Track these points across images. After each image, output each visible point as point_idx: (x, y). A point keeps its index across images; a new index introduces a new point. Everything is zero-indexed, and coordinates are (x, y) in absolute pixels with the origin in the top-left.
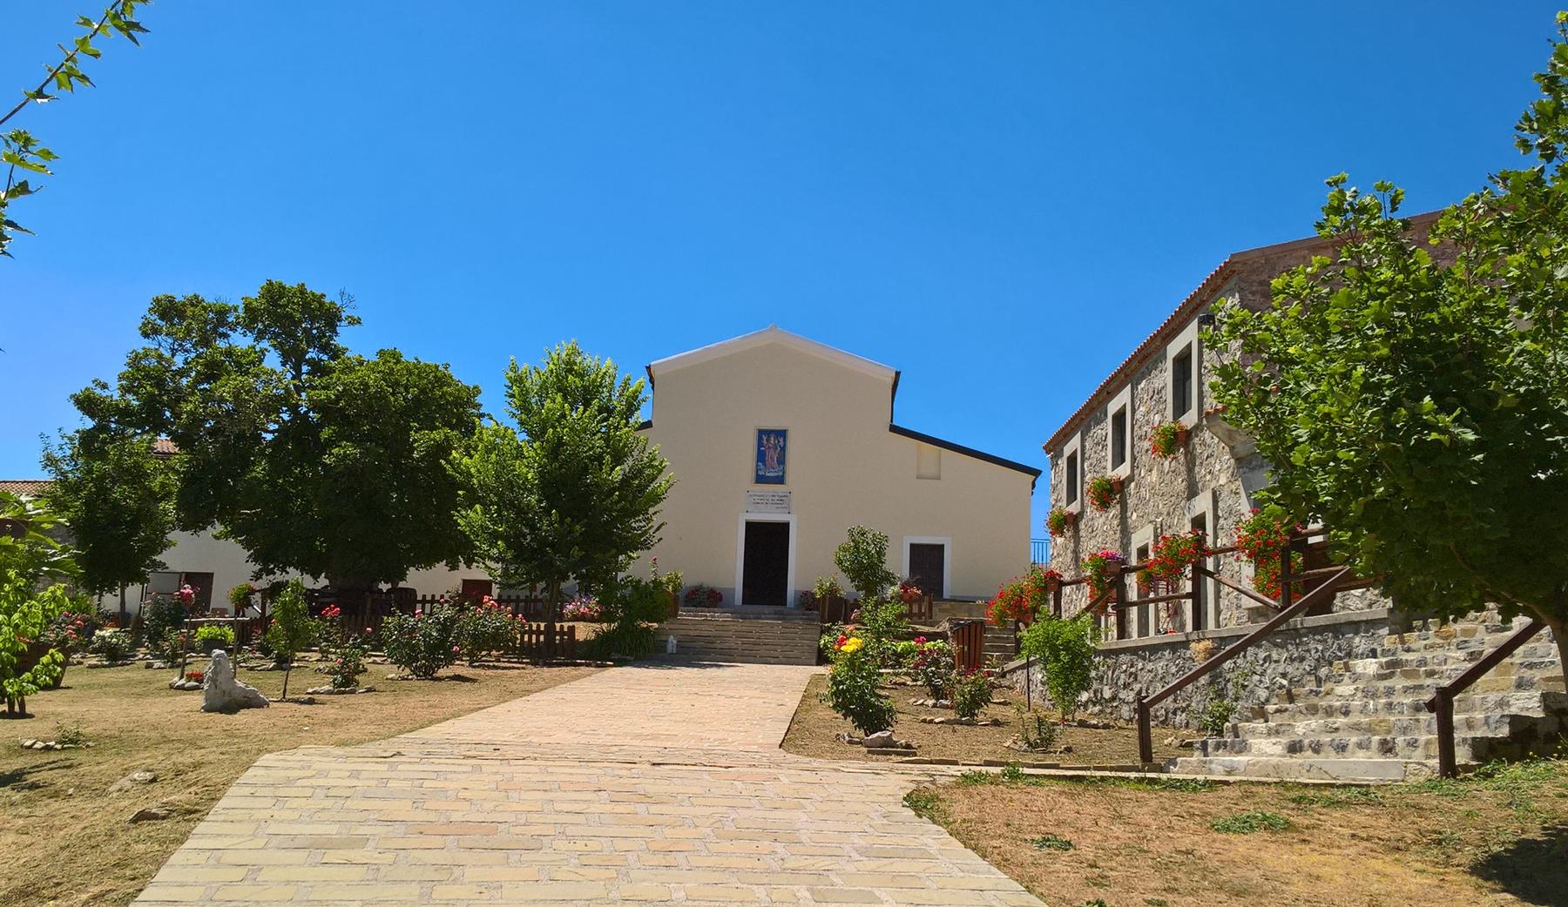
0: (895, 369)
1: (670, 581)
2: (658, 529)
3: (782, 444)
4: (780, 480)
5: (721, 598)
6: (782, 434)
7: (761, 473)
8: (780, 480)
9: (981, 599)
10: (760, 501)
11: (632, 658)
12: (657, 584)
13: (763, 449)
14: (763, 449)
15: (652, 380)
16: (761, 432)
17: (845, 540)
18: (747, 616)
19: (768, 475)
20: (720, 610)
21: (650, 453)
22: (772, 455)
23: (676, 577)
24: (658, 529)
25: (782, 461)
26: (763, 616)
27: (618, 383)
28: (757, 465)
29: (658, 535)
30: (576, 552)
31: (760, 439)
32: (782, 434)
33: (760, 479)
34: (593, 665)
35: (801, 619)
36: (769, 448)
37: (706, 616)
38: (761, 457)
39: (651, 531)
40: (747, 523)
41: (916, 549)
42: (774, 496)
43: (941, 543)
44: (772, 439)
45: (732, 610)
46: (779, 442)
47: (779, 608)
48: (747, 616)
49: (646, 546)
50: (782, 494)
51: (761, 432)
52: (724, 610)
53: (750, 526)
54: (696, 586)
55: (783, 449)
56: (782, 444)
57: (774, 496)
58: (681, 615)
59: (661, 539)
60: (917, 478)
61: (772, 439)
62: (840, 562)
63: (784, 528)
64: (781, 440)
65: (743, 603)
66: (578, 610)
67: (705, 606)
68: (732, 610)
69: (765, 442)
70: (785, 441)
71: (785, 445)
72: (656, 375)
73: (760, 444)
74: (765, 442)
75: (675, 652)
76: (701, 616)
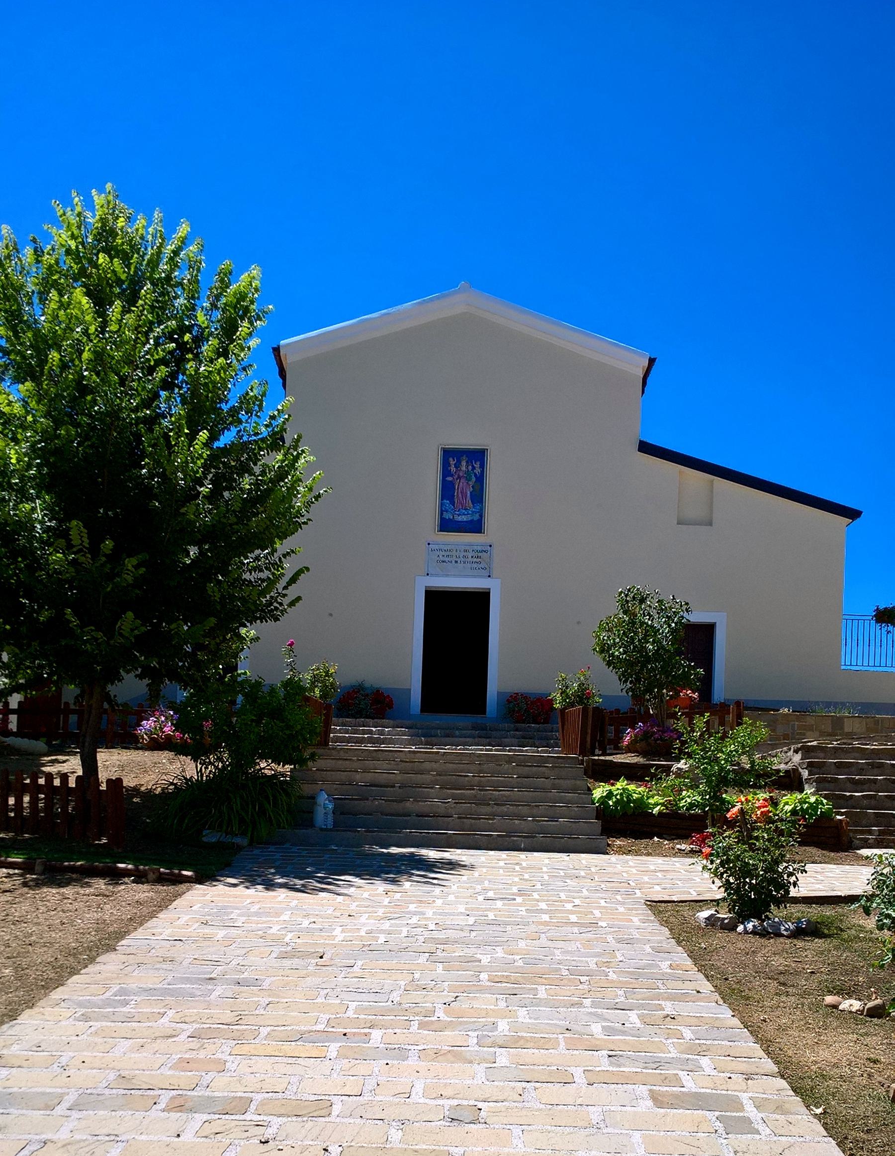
0: (648, 355)
1: (315, 679)
2: (293, 580)
3: (478, 471)
4: (476, 527)
5: (390, 705)
6: (478, 456)
7: (447, 516)
8: (476, 527)
9: (787, 704)
10: (447, 559)
11: (244, 842)
12: (293, 687)
13: (449, 479)
14: (449, 479)
15: (282, 373)
16: (448, 454)
17: (613, 610)
18: (433, 732)
19: (460, 518)
20: (391, 722)
21: (273, 418)
22: (464, 488)
23: (327, 673)
24: (293, 580)
25: (478, 497)
26: (457, 733)
27: (209, 282)
28: (442, 505)
29: (293, 592)
30: (128, 621)
31: (445, 465)
32: (478, 456)
33: (446, 525)
34: (151, 876)
35: (514, 737)
36: (459, 477)
37: (371, 732)
38: (447, 491)
39: (280, 586)
40: (427, 592)
41: (640, 450)
42: (466, 551)
43: (712, 621)
44: (464, 463)
45: (407, 722)
46: (474, 468)
47: (477, 719)
48: (433, 732)
49: (269, 613)
50: (479, 548)
51: (448, 454)
52: (398, 722)
53: (434, 598)
54: (352, 687)
55: (481, 479)
56: (478, 471)
57: (466, 551)
58: (335, 731)
59: (299, 599)
60: (678, 524)
61: (464, 463)
62: (604, 649)
63: (483, 598)
64: (477, 465)
65: (422, 710)
66: (161, 729)
67: (367, 717)
68: (407, 722)
69: (453, 469)
70: (482, 466)
71: (482, 472)
72: (289, 360)
73: (446, 472)
74: (453, 469)
75: (330, 827)
76: (364, 732)
